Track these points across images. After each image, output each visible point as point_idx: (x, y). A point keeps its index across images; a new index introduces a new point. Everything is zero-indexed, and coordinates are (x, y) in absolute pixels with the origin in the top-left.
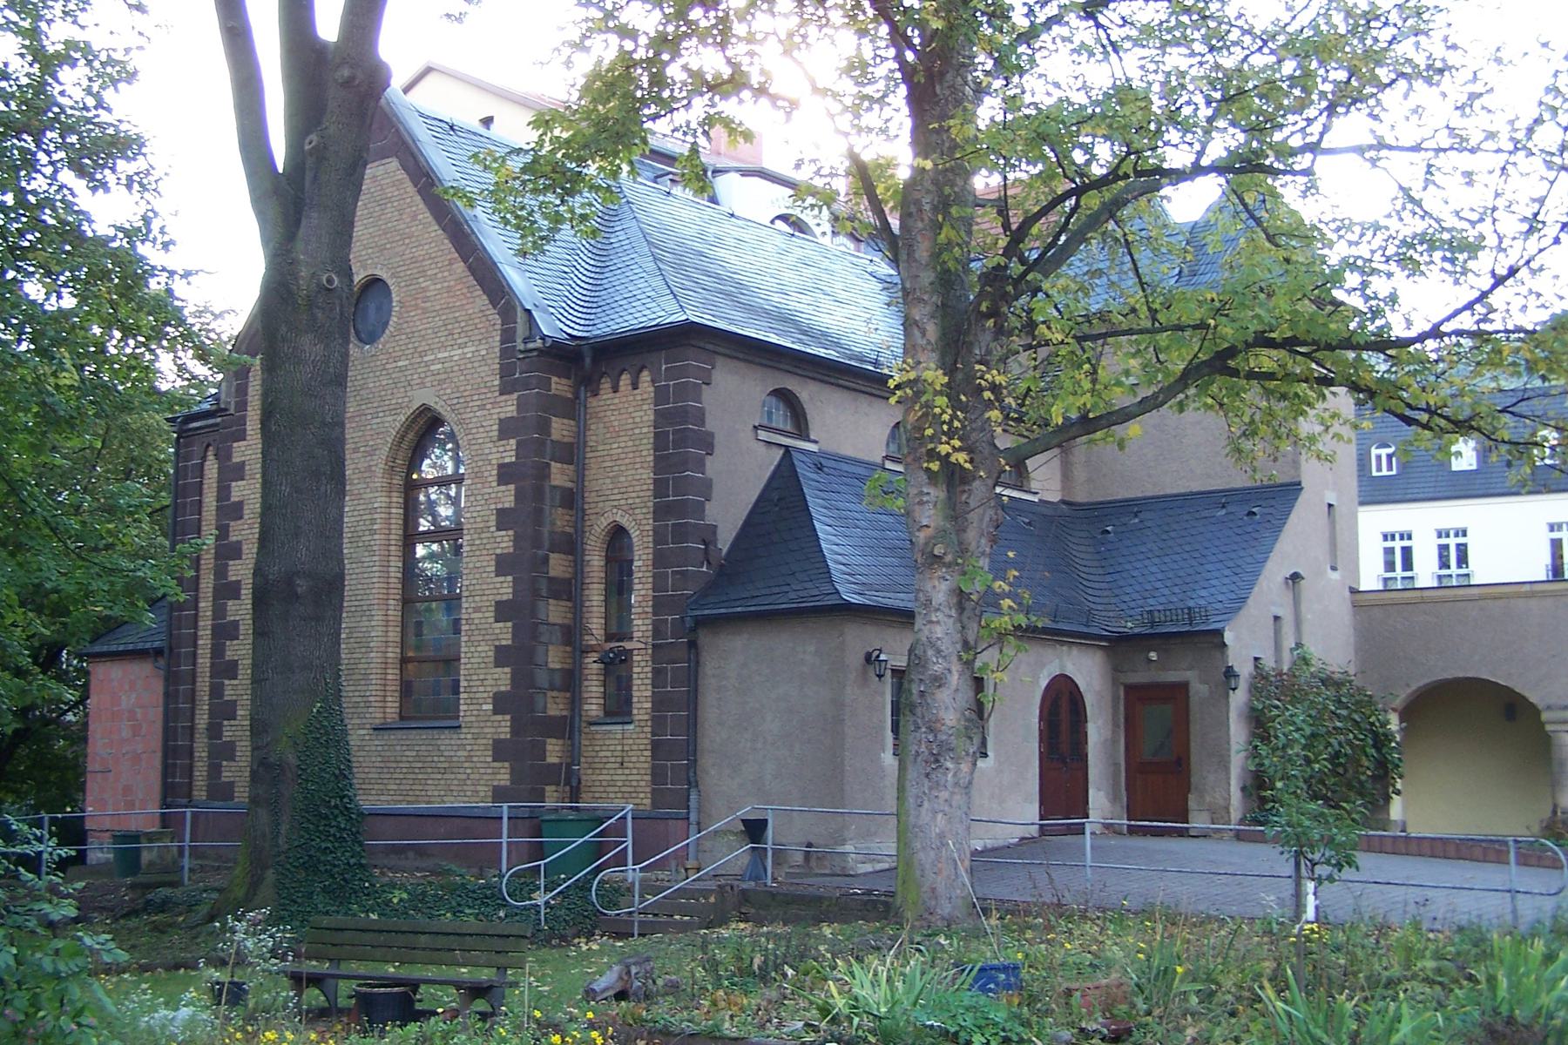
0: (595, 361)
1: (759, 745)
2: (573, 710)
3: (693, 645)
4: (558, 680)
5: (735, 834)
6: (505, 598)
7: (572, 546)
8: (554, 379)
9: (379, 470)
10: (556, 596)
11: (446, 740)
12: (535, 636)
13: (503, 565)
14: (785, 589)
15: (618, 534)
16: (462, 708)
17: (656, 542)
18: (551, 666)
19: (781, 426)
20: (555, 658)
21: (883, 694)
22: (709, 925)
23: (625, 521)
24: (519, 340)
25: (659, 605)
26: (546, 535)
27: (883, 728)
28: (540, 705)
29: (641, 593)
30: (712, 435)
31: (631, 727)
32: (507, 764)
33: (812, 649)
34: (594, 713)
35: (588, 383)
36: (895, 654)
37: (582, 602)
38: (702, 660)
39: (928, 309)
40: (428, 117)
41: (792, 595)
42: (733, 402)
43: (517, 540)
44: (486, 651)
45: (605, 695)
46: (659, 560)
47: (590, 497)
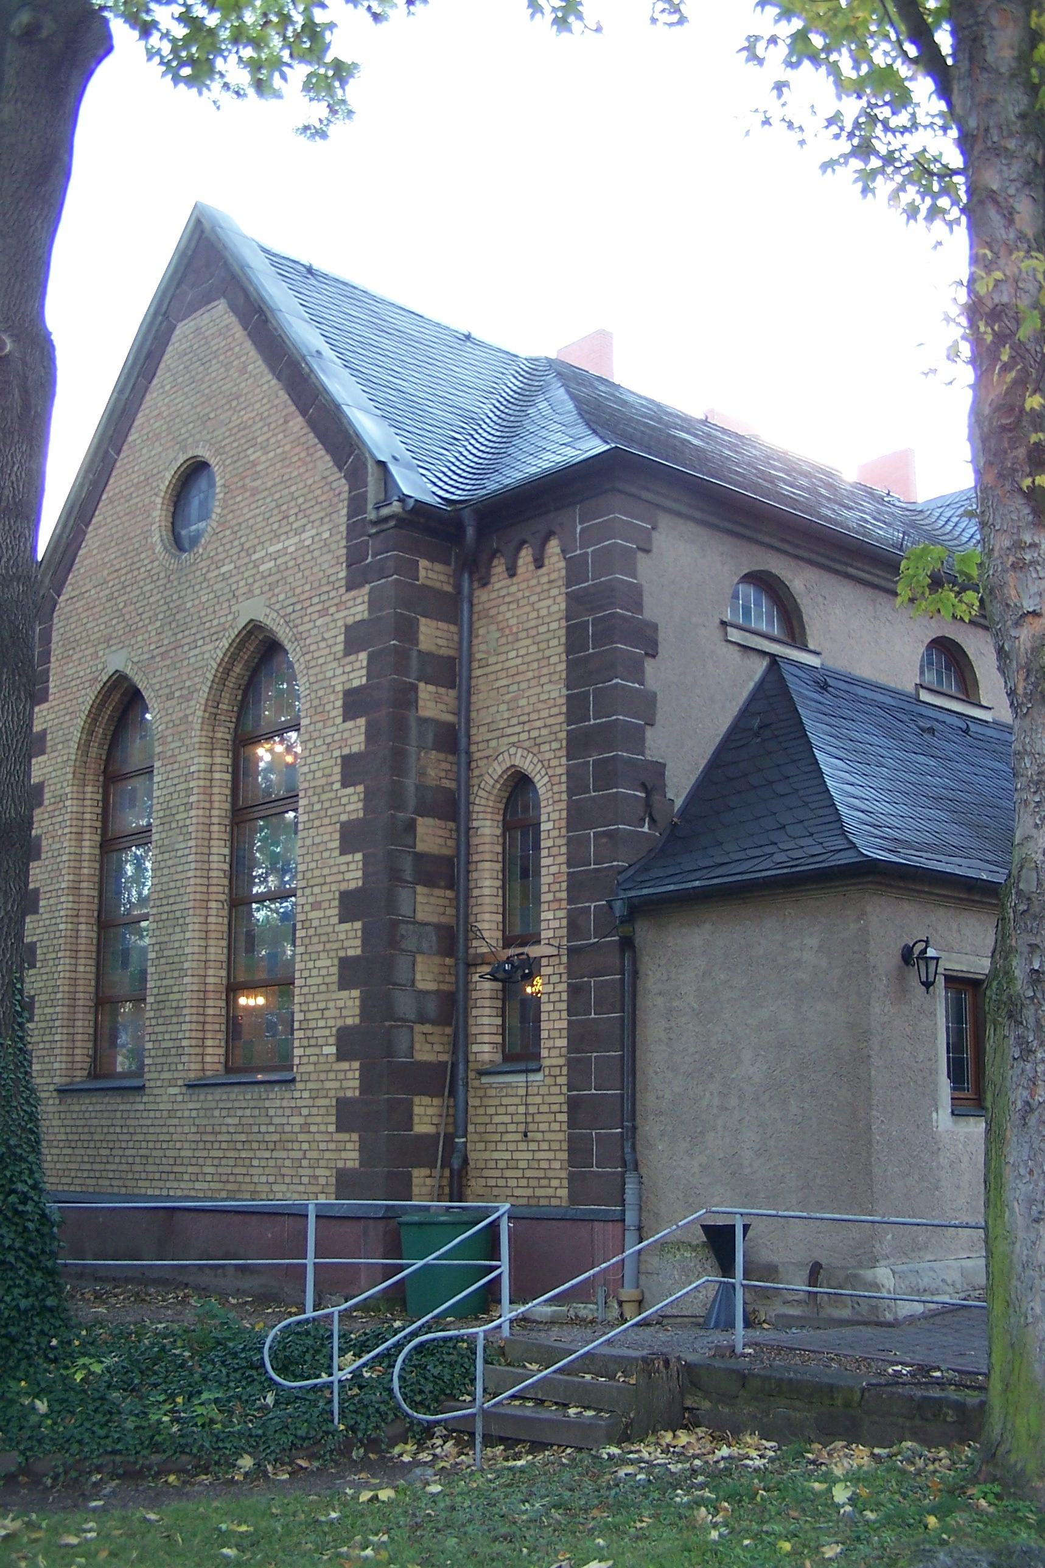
0: (480, 533)
1: (733, 1102)
2: (454, 1052)
3: (627, 944)
4: (432, 1008)
5: (694, 1248)
6: (353, 885)
7: (452, 807)
8: (423, 563)
9: (196, 720)
10: (429, 882)
11: (277, 1098)
12: (393, 942)
13: (351, 837)
14: (769, 850)
15: (519, 785)
16: (297, 1052)
17: (570, 792)
18: (421, 985)
19: (764, 627)
20: (427, 974)
21: (933, 1014)
22: (624, 1438)
23: (528, 765)
24: (370, 507)
25: (576, 887)
26: (412, 790)
27: (933, 1072)
28: (403, 1046)
29: (552, 866)
30: (655, 627)
31: (539, 1077)
32: (355, 1137)
33: (813, 942)
34: (487, 1057)
35: (474, 567)
36: (951, 950)
37: (468, 890)
38: (642, 969)
39: (1017, 168)
40: (275, 255)
41: (780, 857)
42: (684, 575)
43: (368, 799)
44: (327, 966)
45: (504, 1030)
46: (577, 817)
47: (479, 734)
